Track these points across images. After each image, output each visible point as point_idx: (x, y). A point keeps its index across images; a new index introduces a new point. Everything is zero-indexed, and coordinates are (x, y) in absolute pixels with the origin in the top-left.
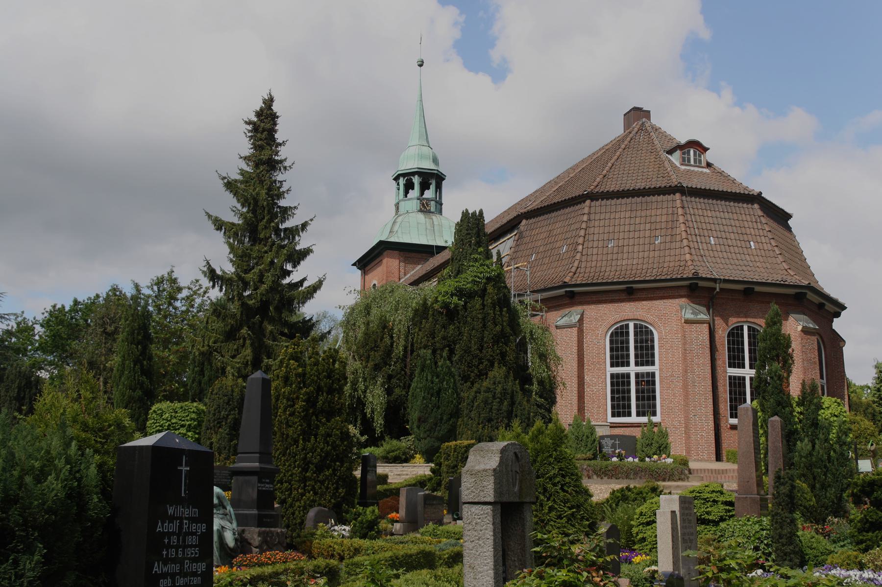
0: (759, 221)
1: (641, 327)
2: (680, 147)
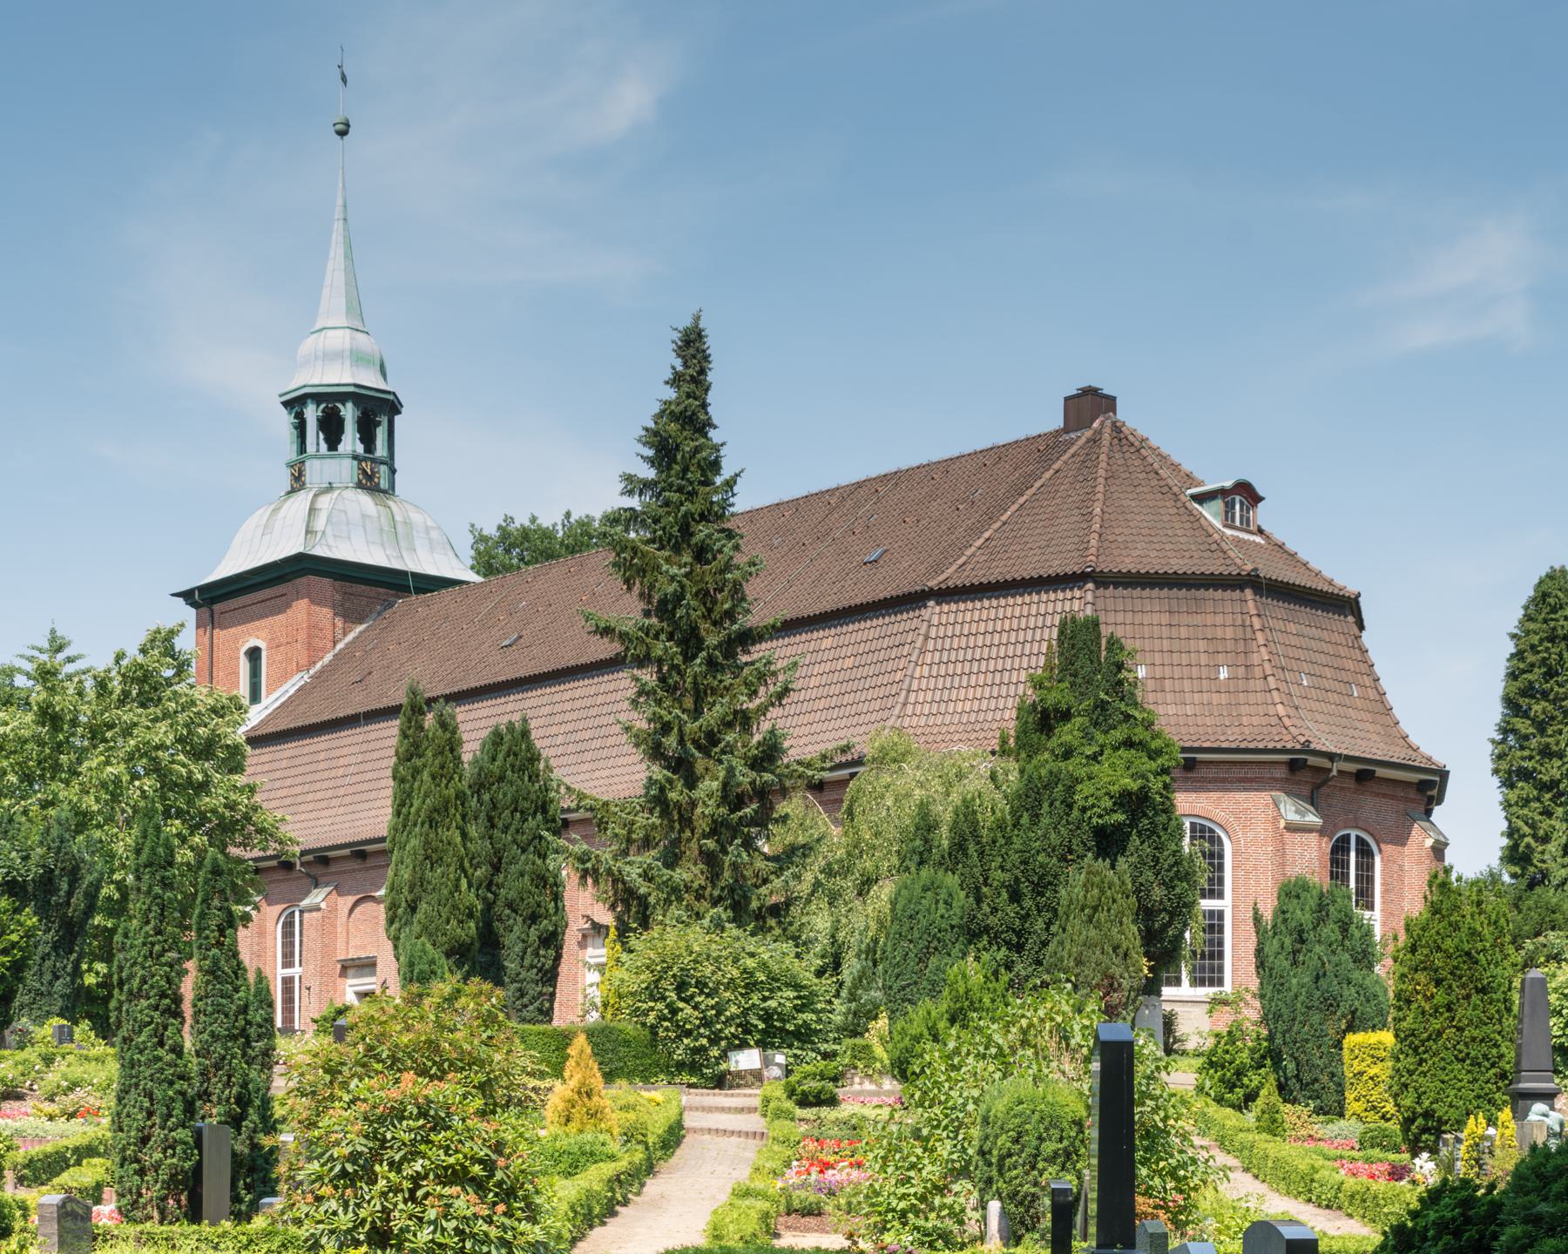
0: (1248, 623)
1: (1203, 828)
2: (1221, 493)
